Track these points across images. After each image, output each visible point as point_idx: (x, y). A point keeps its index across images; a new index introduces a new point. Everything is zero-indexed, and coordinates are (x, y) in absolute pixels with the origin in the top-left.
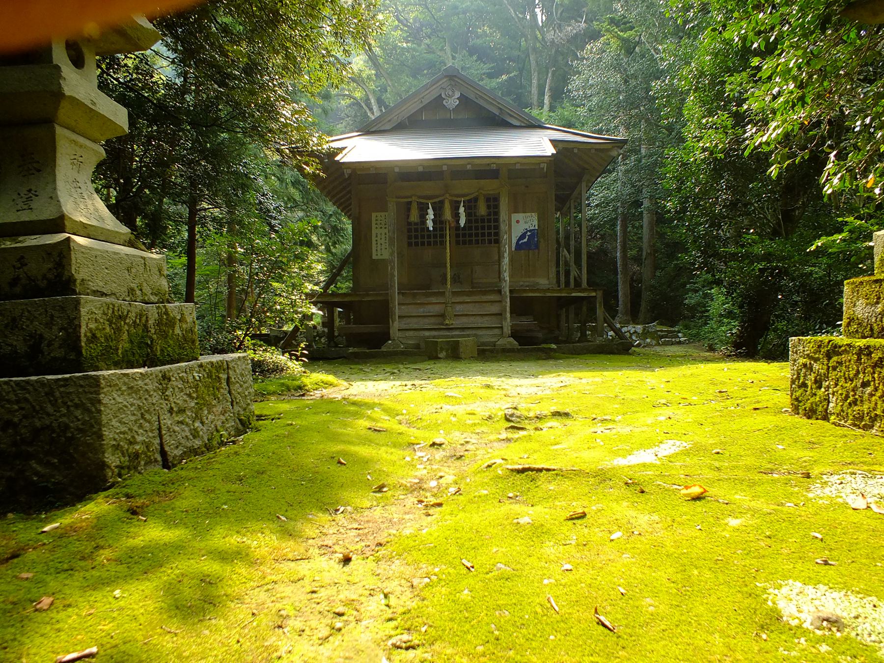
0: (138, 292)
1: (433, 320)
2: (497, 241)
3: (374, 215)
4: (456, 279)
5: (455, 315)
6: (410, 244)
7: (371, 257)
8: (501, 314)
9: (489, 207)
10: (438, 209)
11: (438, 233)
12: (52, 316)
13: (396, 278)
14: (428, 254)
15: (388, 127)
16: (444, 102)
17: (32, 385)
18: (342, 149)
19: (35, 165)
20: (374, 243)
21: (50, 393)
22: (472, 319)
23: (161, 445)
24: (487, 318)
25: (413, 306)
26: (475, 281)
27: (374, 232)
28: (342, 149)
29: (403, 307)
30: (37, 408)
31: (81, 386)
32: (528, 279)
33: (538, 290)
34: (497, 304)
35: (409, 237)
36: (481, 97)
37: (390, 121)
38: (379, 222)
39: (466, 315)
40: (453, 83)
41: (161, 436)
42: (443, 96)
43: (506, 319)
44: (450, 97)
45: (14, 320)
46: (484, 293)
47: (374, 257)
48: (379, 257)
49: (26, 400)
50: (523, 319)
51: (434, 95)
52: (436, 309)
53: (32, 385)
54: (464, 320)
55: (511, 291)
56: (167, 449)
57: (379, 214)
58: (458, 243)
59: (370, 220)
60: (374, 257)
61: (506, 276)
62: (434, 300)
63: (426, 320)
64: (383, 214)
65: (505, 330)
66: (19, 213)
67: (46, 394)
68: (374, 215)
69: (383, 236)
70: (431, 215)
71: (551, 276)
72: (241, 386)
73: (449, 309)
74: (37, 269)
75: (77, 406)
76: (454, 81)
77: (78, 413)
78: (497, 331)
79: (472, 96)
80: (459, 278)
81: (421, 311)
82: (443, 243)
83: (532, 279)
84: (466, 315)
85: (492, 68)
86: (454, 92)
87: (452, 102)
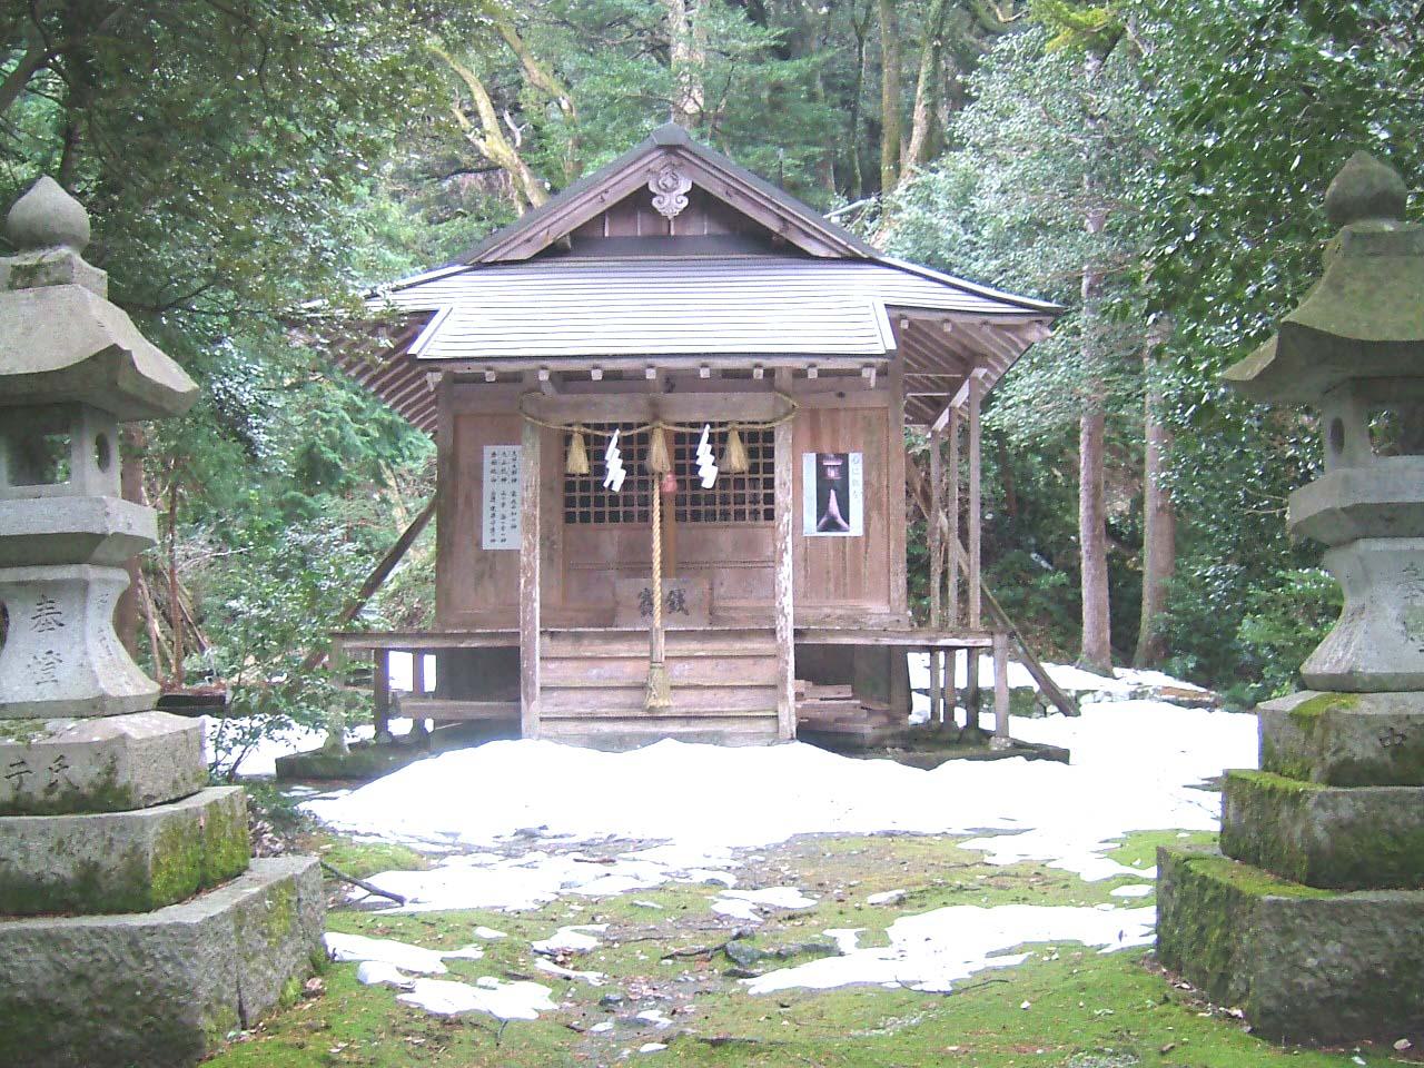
0: (182, 783)
1: (620, 697)
2: (770, 515)
3: (488, 450)
4: (674, 604)
5: (672, 688)
6: (569, 518)
7: (479, 544)
8: (774, 687)
9: (752, 453)
10: (634, 453)
11: (635, 493)
12: (111, 839)
13: (537, 605)
14: (610, 539)
15: (524, 254)
16: (655, 202)
17: (111, 933)
18: (424, 317)
19: (57, 617)
20: (486, 513)
21: (133, 943)
22: (708, 694)
23: (240, 1002)
24: (742, 694)
25: (575, 664)
26: (716, 603)
27: (488, 487)
28: (424, 317)
29: (552, 666)
30: (117, 960)
31: (172, 935)
32: (842, 602)
33: (861, 632)
34: (768, 661)
35: (569, 502)
36: (738, 192)
37: (529, 240)
38: (499, 467)
39: (697, 687)
40: (675, 160)
41: (239, 991)
42: (653, 188)
43: (784, 697)
44: (667, 190)
45: (61, 843)
46: (741, 635)
47: (487, 545)
48: (498, 546)
49: (105, 951)
50: (829, 692)
51: (633, 185)
52: (629, 672)
53: (111, 933)
54: (691, 697)
55: (797, 633)
56: (245, 1007)
57: (499, 449)
58: (680, 517)
59: (480, 467)
60: (487, 545)
61: (787, 602)
62: (621, 648)
63: (606, 697)
64: (509, 449)
65: (784, 722)
66: (40, 687)
67: (130, 944)
68: (488, 450)
69: (509, 498)
70: (613, 459)
71: (894, 595)
72: (313, 909)
73: (658, 674)
74: (83, 774)
75: (166, 959)
76: (678, 155)
77: (168, 967)
78: (765, 726)
79: (718, 190)
80: (681, 601)
81: (595, 674)
82: (646, 517)
83: (852, 602)
84: (697, 687)
85: (780, 38)
86: (676, 180)
87: (672, 202)
